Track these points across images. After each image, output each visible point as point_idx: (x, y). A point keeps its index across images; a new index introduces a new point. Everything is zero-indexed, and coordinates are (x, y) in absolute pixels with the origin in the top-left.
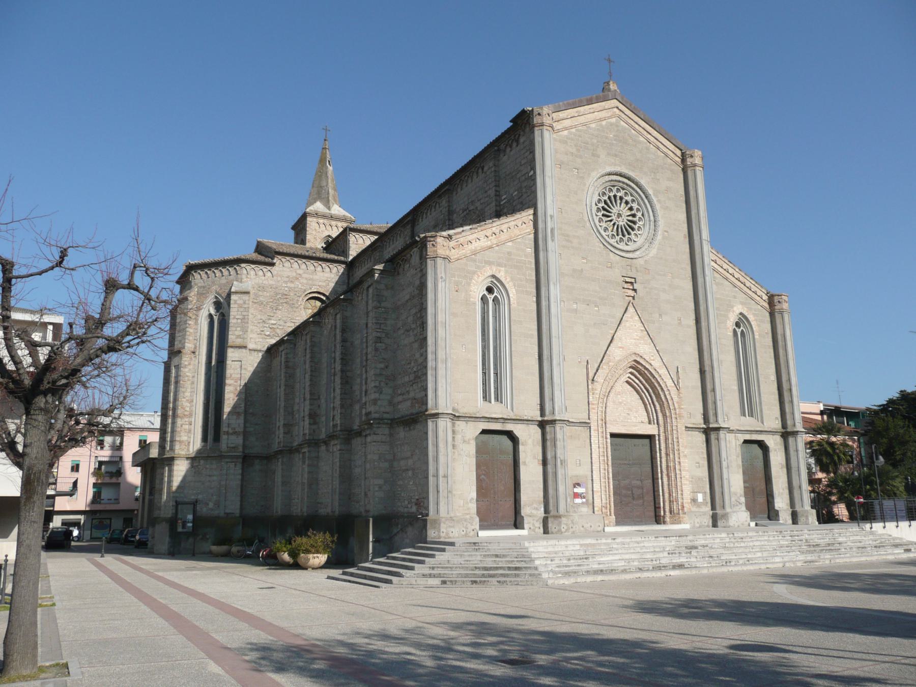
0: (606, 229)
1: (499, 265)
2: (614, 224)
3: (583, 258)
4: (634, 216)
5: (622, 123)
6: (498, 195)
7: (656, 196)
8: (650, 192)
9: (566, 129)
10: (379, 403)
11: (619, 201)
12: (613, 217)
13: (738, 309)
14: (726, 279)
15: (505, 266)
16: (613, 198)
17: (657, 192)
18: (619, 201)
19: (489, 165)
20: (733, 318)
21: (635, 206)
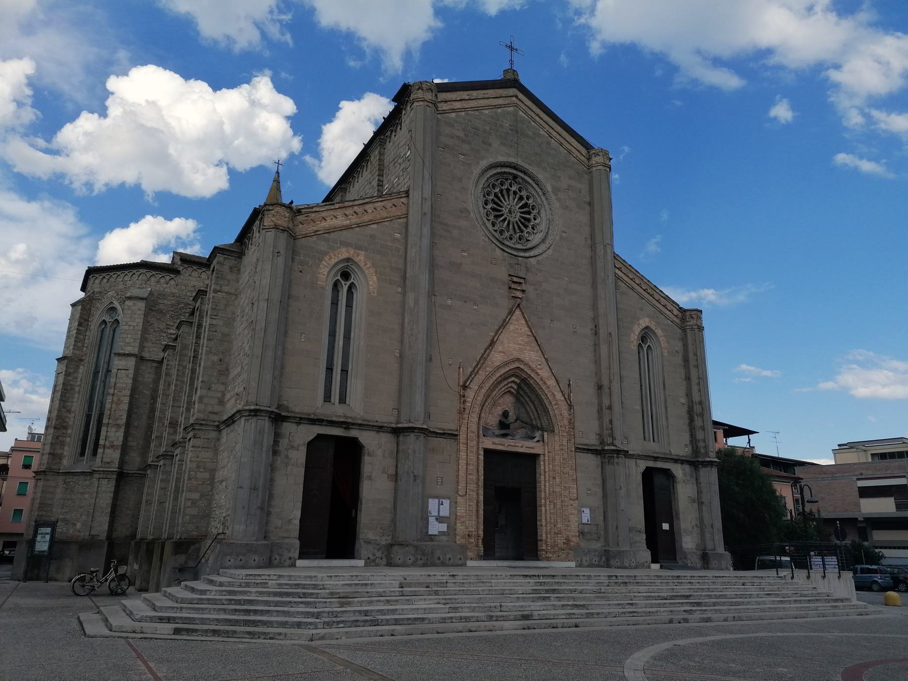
1: (358, 247)
2: (508, 224)
3: (463, 251)
5: (521, 113)
6: (380, 185)
7: (556, 194)
9: (454, 110)
10: (205, 400)
11: (511, 198)
13: (644, 322)
14: (633, 289)
15: (366, 250)
17: (556, 190)
19: (374, 156)
20: (637, 330)
21: (524, 193)
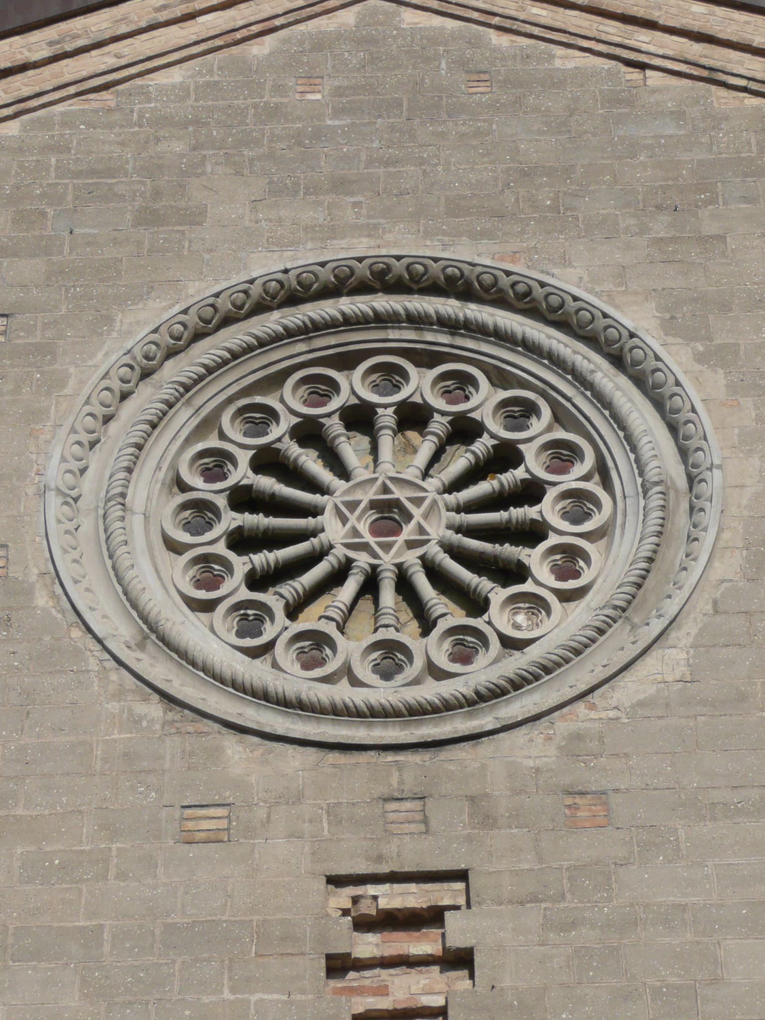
0: (390, 656)
4: (464, 430)
8: (637, 318)
11: (311, 462)
12: (387, 561)
16: (267, 483)
18: (311, 462)
